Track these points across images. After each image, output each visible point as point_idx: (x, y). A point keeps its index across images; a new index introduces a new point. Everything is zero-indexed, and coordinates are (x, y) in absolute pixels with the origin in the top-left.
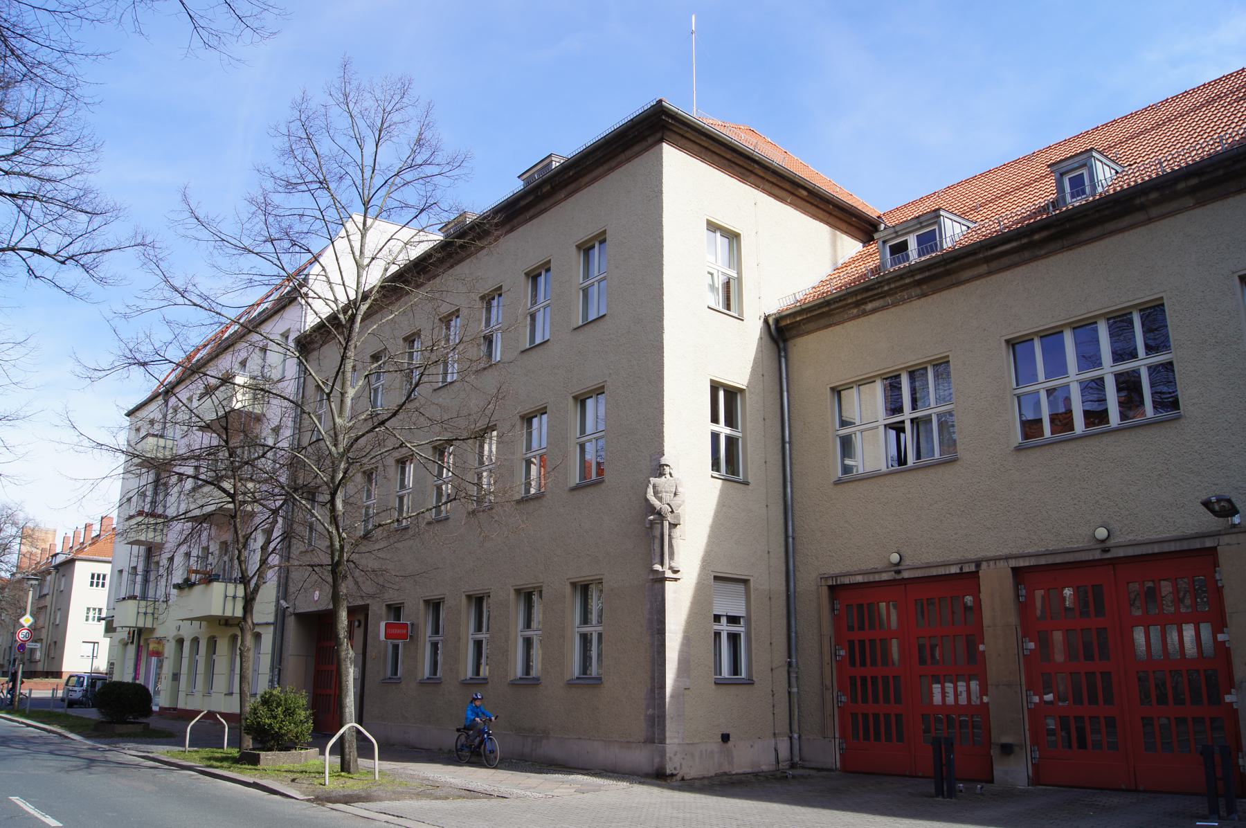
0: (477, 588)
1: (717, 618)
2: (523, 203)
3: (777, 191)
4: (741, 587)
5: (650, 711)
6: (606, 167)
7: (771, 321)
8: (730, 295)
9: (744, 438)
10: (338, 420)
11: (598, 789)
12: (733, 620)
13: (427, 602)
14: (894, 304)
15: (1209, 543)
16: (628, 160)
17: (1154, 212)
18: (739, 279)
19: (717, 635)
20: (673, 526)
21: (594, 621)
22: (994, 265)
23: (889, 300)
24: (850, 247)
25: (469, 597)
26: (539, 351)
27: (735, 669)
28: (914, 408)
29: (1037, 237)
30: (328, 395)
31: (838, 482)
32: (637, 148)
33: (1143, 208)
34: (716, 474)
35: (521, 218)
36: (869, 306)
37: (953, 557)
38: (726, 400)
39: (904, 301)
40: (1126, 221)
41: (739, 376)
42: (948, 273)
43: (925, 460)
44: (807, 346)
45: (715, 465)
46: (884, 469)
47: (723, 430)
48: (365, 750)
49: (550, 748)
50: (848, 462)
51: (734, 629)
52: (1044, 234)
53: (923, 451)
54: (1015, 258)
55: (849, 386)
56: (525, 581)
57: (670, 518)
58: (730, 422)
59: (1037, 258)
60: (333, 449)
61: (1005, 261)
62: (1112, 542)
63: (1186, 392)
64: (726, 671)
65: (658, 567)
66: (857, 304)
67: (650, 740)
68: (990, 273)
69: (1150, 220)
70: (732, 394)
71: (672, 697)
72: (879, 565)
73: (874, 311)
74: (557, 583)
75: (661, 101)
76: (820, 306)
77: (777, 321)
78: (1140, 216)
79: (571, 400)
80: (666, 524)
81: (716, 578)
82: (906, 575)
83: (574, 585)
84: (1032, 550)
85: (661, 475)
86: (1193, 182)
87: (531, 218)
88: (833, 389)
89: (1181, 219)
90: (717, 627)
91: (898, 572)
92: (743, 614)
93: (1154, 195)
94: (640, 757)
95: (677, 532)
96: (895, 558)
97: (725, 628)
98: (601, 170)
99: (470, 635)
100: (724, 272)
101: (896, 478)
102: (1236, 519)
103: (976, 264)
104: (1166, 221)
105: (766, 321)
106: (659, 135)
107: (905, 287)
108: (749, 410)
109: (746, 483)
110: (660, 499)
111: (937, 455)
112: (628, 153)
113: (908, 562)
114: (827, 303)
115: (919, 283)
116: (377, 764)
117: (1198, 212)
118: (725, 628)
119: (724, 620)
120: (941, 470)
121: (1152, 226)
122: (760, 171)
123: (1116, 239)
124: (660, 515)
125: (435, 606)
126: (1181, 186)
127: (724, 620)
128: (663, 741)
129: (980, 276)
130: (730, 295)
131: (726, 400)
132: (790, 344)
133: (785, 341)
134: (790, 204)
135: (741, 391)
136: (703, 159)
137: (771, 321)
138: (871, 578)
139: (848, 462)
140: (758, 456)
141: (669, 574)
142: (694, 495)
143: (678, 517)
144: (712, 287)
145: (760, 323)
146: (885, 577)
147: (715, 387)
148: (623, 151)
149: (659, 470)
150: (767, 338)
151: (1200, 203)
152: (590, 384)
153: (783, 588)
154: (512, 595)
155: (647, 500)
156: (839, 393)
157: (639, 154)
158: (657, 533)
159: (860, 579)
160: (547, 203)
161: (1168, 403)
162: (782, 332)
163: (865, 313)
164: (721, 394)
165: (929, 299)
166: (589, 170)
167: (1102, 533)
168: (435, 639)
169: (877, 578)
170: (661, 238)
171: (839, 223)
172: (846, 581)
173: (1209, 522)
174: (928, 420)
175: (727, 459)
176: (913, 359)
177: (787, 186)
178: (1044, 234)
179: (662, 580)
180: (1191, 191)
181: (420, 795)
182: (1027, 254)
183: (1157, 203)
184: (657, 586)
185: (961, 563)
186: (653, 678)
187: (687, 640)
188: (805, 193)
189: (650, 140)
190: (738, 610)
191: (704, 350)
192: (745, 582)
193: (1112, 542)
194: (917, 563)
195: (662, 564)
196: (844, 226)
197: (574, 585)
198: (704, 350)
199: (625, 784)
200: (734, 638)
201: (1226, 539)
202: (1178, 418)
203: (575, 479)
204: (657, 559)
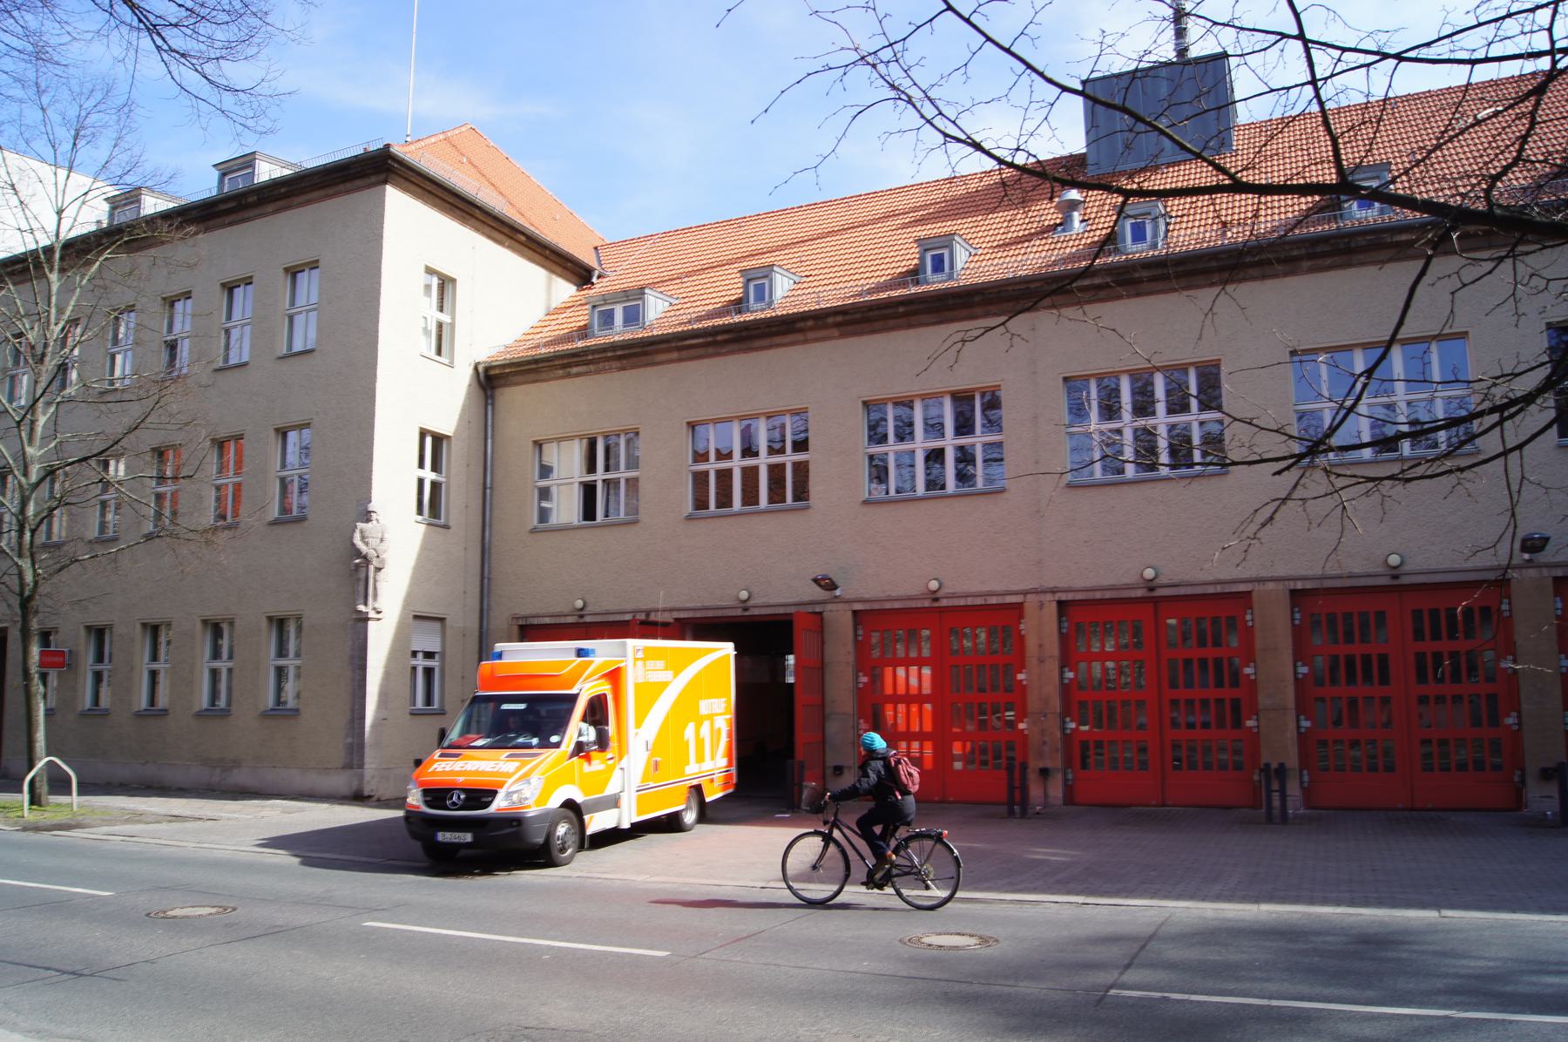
0: (154, 617)
1: (414, 654)
2: (223, 207)
3: (496, 234)
4: (437, 625)
5: (349, 740)
6: (322, 193)
7: (481, 369)
8: (442, 340)
9: (448, 483)
10: (29, 450)
11: (302, 810)
12: (429, 655)
13: (89, 628)
14: (598, 372)
15: (818, 609)
16: (348, 192)
17: (811, 335)
18: (452, 325)
19: (414, 669)
20: (378, 569)
21: (292, 654)
22: (684, 354)
23: (592, 367)
24: (565, 290)
25: (144, 625)
26: (236, 373)
27: (429, 700)
28: (607, 469)
29: (719, 338)
30: (19, 423)
31: (534, 531)
32: (358, 183)
33: (801, 330)
34: (420, 518)
35: (218, 221)
36: (575, 370)
37: (630, 607)
38: (435, 446)
39: (604, 371)
40: (777, 340)
41: (446, 424)
42: (646, 354)
43: (612, 518)
44: (513, 397)
45: (420, 511)
46: (576, 522)
47: (429, 475)
48: (59, 784)
49: (241, 777)
50: (545, 504)
51: (429, 663)
52: (725, 337)
53: (611, 511)
54: (701, 351)
55: (550, 441)
56: (214, 612)
57: (375, 563)
58: (436, 467)
59: (718, 355)
60: (23, 480)
61: (693, 352)
62: (751, 603)
63: (815, 487)
64: (420, 703)
65: (361, 608)
66: (564, 366)
67: (348, 766)
68: (680, 360)
69: (806, 342)
70: (438, 439)
71: (373, 726)
72: (566, 610)
73: (578, 375)
74: (251, 616)
75: (388, 146)
76: (529, 362)
77: (487, 369)
78: (799, 337)
79: (272, 433)
80: (372, 568)
81: (416, 617)
82: (588, 619)
83: (270, 619)
84: (689, 605)
85: (368, 520)
86: (839, 319)
87: (231, 224)
88: (535, 442)
89: (828, 345)
90: (414, 662)
91: (582, 616)
92: (437, 649)
93: (810, 323)
94: (340, 781)
95: (381, 575)
96: (579, 604)
97: (421, 662)
98: (316, 194)
99: (144, 665)
100: (441, 317)
101: (585, 533)
102: (838, 592)
103: (669, 350)
104: (817, 344)
105: (476, 368)
106: (383, 176)
107: (608, 359)
108: (455, 456)
109: (446, 527)
110: (367, 544)
111: (622, 515)
112: (349, 185)
113: (590, 609)
114: (536, 361)
115: (620, 358)
116: (75, 798)
117: (841, 342)
118: (421, 662)
119: (420, 656)
120: (623, 529)
121: (808, 346)
122: (482, 217)
123: (781, 351)
124: (366, 559)
125: (99, 634)
126: (830, 320)
127: (420, 656)
128: (361, 766)
129: (671, 361)
130: (442, 340)
131: (435, 446)
132: (498, 392)
133: (493, 388)
134: (508, 247)
135: (448, 437)
136: (426, 201)
137: (481, 369)
138: (558, 620)
139: (545, 504)
140: (460, 502)
141: (372, 614)
142: (397, 537)
143: (383, 561)
144: (426, 331)
145: (470, 371)
146: (570, 620)
147: (423, 433)
148: (344, 182)
149: (367, 516)
150: (475, 384)
151: (843, 335)
152: (296, 419)
153: (477, 625)
154: (199, 626)
155: (353, 545)
156: (540, 446)
157: (359, 189)
158: (363, 576)
159: (547, 621)
160: (252, 213)
161: (801, 493)
162: (491, 380)
163: (569, 376)
164: (429, 440)
165: (628, 373)
166: (302, 192)
167: (744, 595)
168: (99, 667)
169: (562, 620)
170: (379, 284)
171: (554, 267)
172: (535, 621)
173: (818, 593)
174: (617, 482)
175: (432, 503)
176: (609, 427)
177: (506, 230)
178: (725, 337)
179: (365, 619)
180: (838, 325)
181: (127, 821)
182: (711, 350)
183: (812, 329)
184: (360, 624)
185: (635, 612)
186: (353, 711)
187: (387, 676)
188: (523, 238)
189: (373, 179)
190: (434, 646)
191: (415, 395)
192: (442, 620)
193: (751, 603)
194: (598, 610)
195: (366, 604)
196: (559, 270)
197: (270, 619)
198: (415, 395)
199: (325, 806)
200: (429, 672)
201: (829, 607)
202: (808, 508)
203: (274, 512)
204: (361, 600)
